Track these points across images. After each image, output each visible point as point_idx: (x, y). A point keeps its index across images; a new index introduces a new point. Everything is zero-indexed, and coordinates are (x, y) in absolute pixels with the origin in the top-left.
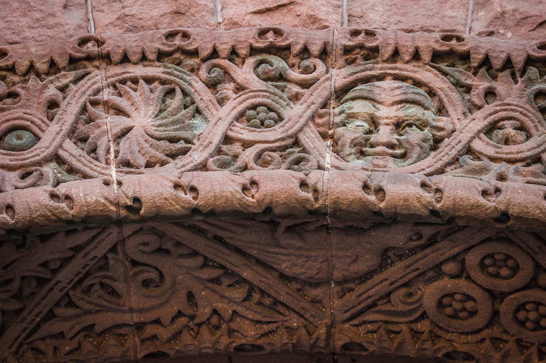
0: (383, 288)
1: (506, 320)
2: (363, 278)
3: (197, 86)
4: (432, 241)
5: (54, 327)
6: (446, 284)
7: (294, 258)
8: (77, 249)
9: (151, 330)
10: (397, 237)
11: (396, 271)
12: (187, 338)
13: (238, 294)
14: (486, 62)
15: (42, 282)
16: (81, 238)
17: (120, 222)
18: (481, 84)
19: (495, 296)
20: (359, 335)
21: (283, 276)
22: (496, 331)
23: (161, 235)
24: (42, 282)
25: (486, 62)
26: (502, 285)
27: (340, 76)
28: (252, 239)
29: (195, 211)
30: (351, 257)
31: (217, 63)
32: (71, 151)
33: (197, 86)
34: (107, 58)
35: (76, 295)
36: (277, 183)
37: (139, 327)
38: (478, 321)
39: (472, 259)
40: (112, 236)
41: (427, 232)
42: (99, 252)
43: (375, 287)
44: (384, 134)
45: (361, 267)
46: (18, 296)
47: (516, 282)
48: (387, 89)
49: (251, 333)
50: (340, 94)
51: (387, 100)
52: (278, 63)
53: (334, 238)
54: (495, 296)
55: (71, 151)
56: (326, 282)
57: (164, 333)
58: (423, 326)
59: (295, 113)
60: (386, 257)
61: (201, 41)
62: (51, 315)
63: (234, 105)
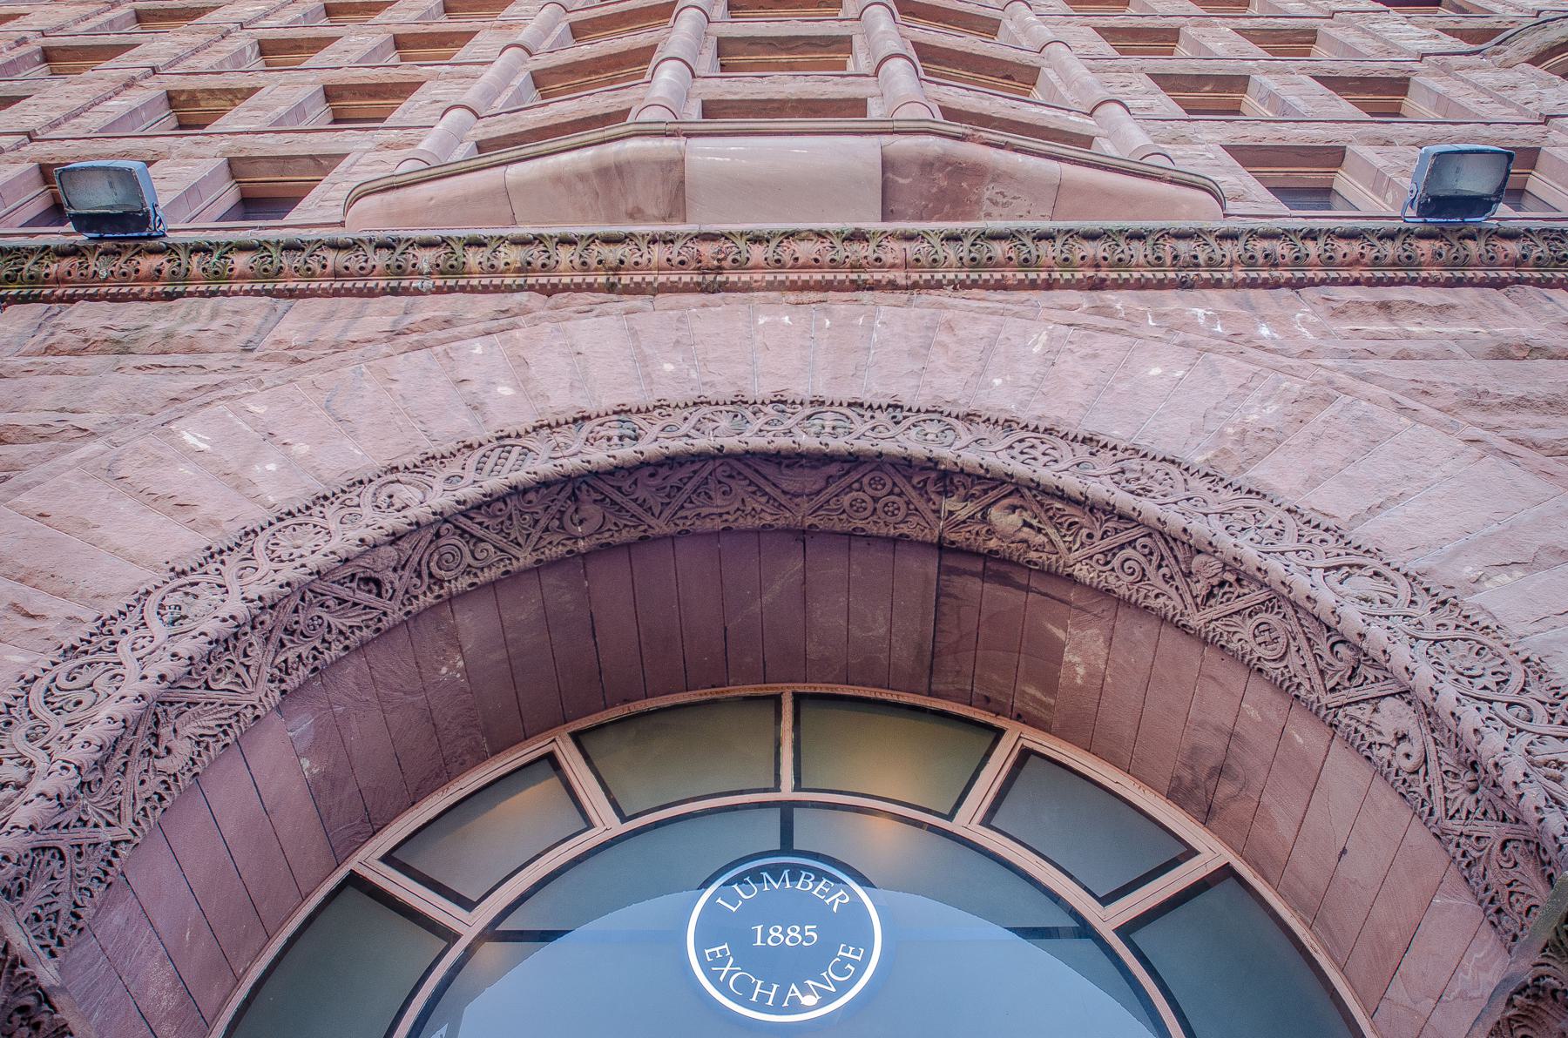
0: (827, 497)
1: (879, 512)
2: (819, 492)
3: (748, 414)
4: (848, 472)
5: (682, 513)
6: (855, 494)
7: (791, 481)
8: (695, 472)
9: (725, 517)
10: (833, 469)
11: (832, 489)
12: (741, 520)
13: (764, 499)
14: (870, 406)
15: (679, 489)
16: (696, 466)
17: (714, 457)
18: (868, 414)
19: (875, 500)
20: (815, 521)
21: (784, 492)
22: (875, 518)
23: (732, 468)
24: (679, 489)
25: (870, 406)
26: (879, 494)
27: (809, 411)
28: (768, 470)
29: (747, 452)
30: (810, 480)
31: (756, 406)
32: (693, 433)
33: (748, 414)
34: (709, 403)
35: (694, 497)
36: (783, 443)
37: (720, 515)
38: (867, 513)
39: (866, 480)
40: (710, 466)
41: (847, 466)
42: (705, 474)
43: (823, 497)
44: (828, 430)
45: (816, 487)
46: (668, 496)
47: (885, 492)
48: (829, 416)
49: (768, 519)
50: (809, 417)
51: (829, 419)
52: (782, 406)
53: (806, 471)
54: (875, 500)
55: (693, 433)
56: (800, 495)
57: (731, 518)
58: (844, 516)
59: (789, 423)
60: (829, 479)
61: (750, 398)
62: (682, 507)
63: (763, 419)
